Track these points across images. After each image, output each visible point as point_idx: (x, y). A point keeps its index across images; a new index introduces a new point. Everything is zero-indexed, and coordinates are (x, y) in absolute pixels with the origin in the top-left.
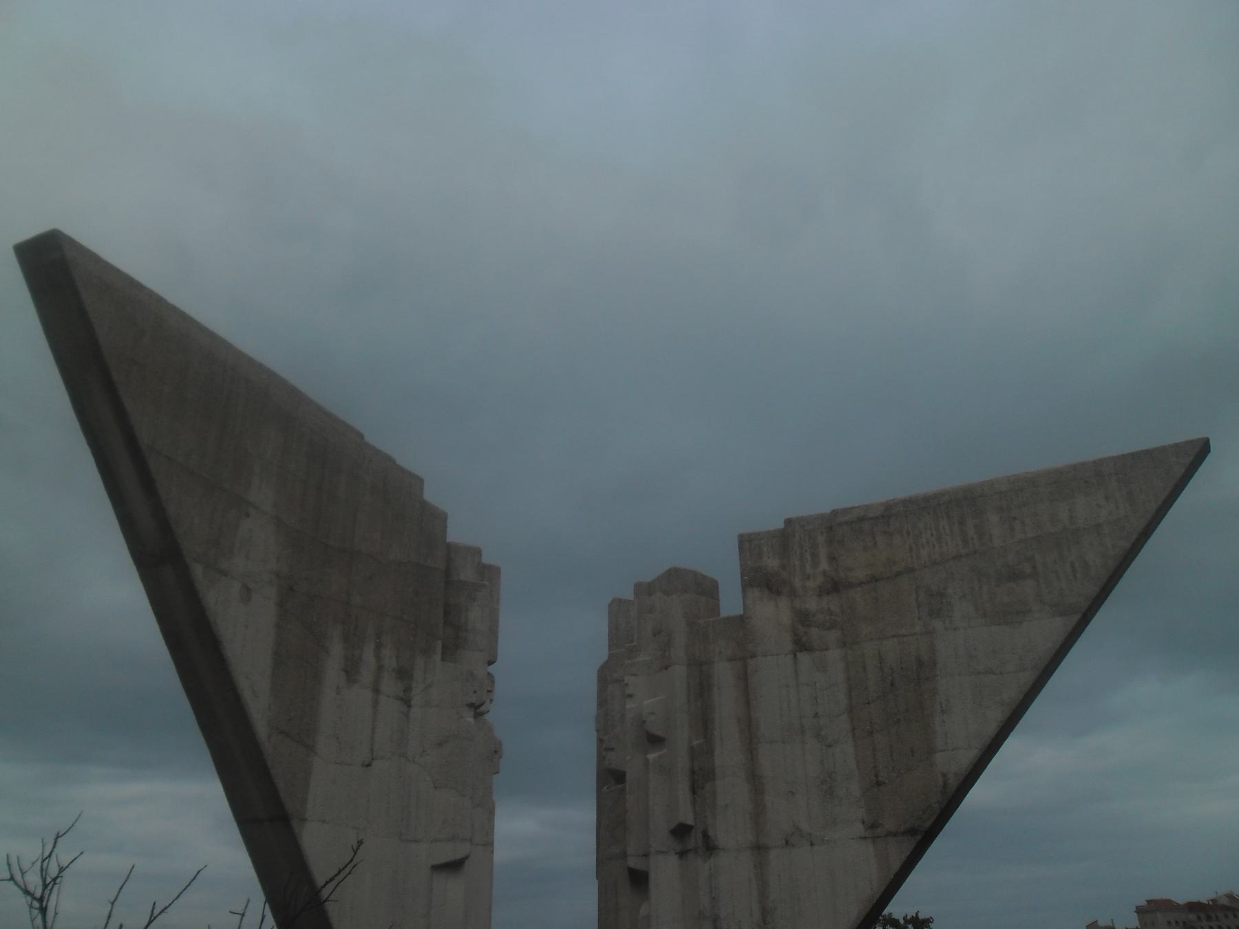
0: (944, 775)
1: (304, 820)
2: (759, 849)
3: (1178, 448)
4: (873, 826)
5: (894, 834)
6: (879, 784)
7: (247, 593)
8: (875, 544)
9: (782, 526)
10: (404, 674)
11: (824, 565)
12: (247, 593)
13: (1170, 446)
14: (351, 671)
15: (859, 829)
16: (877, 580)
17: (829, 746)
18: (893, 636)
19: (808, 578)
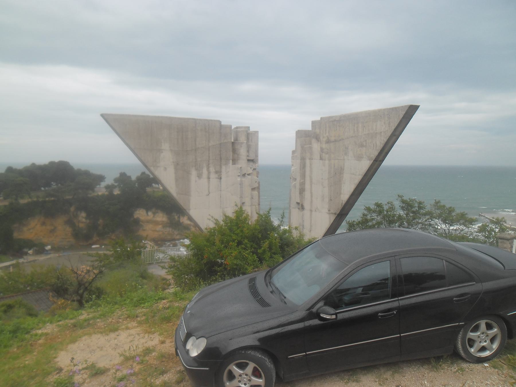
0: (342, 201)
1: (190, 210)
2: (311, 211)
3: (394, 110)
4: (329, 211)
5: (333, 214)
6: (331, 200)
7: (165, 169)
8: (337, 129)
9: (320, 119)
10: (219, 173)
11: (327, 134)
12: (165, 169)
13: (401, 107)
14: (200, 176)
15: (327, 211)
16: (336, 141)
17: (324, 187)
18: (337, 159)
19: (324, 138)
